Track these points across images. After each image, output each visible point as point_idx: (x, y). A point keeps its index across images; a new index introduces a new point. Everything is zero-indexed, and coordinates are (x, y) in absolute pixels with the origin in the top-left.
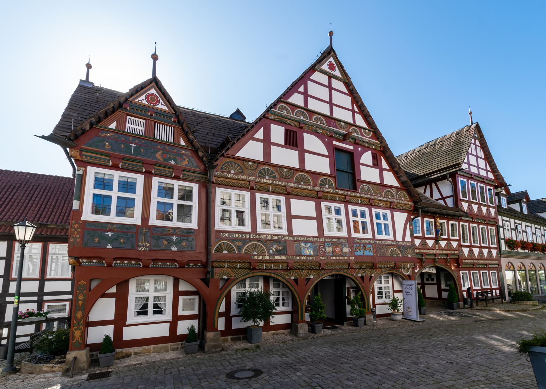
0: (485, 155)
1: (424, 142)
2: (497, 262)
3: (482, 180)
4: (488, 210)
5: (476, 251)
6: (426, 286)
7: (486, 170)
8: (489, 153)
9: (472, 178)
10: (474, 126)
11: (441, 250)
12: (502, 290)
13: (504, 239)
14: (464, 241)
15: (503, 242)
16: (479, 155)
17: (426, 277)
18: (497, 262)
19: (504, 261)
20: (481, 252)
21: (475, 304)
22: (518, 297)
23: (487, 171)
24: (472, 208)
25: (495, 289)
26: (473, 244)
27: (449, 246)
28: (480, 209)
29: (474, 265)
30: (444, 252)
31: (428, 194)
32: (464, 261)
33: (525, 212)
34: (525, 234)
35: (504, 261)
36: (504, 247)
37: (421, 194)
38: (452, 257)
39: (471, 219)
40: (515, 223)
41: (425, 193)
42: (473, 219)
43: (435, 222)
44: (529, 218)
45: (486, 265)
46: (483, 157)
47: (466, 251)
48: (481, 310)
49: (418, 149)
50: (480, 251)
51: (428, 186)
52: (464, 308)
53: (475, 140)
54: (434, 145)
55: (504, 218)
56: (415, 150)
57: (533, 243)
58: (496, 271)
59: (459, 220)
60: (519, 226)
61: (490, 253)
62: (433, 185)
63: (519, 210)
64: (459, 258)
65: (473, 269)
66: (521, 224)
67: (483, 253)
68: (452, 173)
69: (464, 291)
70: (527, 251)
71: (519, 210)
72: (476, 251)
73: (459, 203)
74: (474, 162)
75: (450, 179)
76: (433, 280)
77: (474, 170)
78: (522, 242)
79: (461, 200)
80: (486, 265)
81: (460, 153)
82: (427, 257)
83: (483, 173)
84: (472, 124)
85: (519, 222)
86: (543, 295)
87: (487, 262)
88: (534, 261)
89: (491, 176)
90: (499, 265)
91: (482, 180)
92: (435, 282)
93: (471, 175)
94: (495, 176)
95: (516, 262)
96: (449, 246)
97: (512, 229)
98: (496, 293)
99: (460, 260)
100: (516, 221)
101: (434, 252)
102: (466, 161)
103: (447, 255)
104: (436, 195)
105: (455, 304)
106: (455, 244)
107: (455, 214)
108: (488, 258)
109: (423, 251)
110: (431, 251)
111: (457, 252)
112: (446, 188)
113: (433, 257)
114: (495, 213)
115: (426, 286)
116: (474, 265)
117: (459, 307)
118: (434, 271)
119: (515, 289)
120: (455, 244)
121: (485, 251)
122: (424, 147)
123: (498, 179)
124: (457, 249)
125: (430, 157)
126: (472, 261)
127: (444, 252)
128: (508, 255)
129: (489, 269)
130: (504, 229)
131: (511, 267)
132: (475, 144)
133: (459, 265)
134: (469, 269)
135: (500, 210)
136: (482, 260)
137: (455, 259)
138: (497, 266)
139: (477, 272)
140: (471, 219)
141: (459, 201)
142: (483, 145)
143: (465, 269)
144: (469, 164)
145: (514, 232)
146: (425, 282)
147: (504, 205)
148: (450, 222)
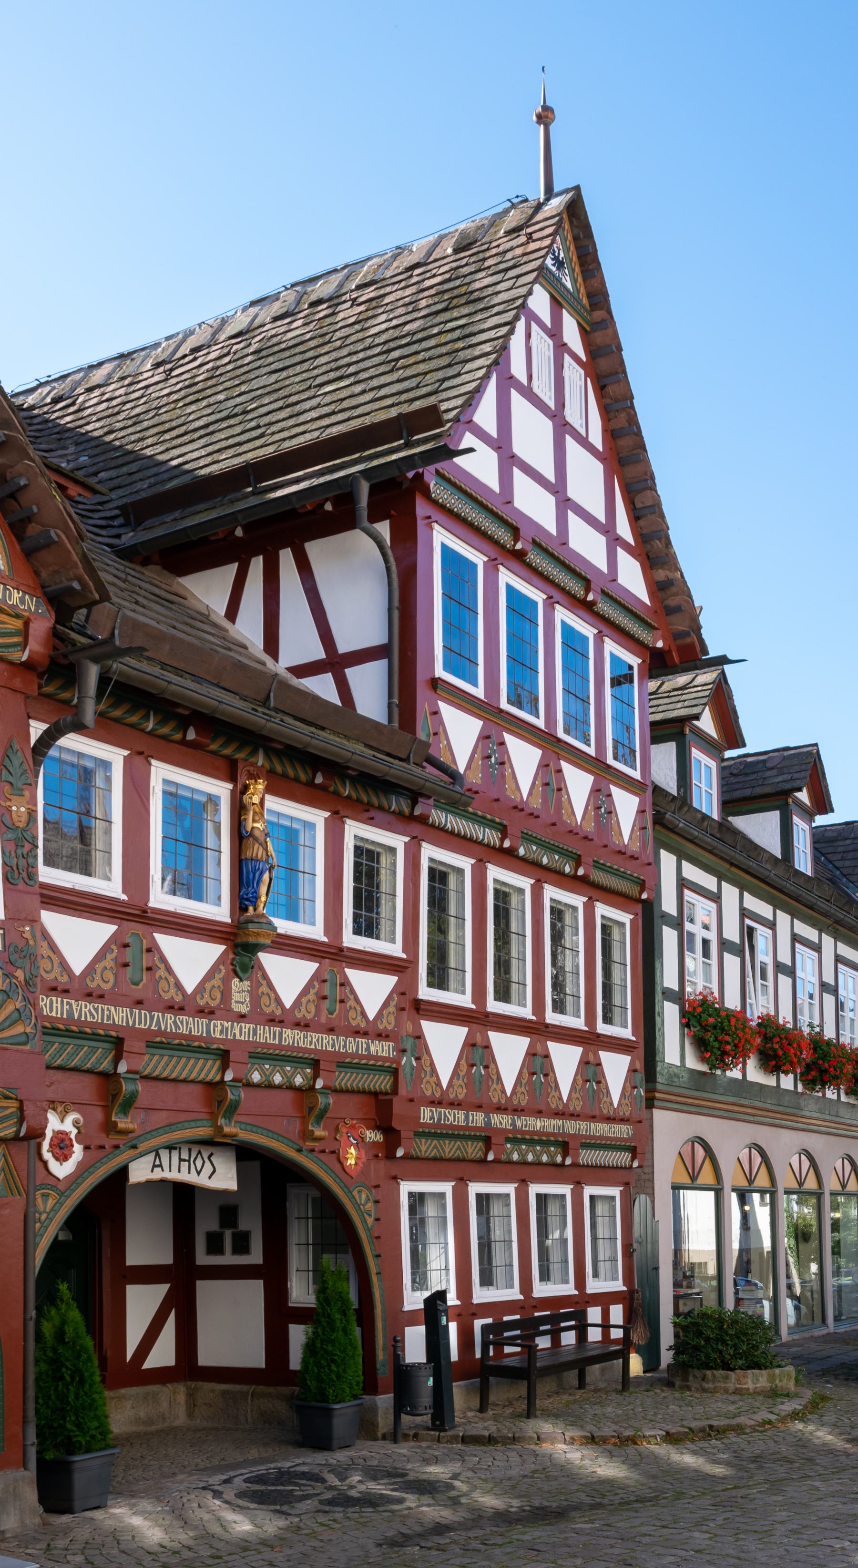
0: (610, 433)
1: (276, 275)
2: (623, 1131)
3: (576, 588)
4: (599, 797)
5: (509, 1052)
6: (205, 1289)
7: (607, 529)
8: (633, 420)
9: (519, 556)
10: (556, 204)
11: (272, 1021)
12: (639, 1303)
13: (678, 997)
14: (438, 979)
15: (670, 1015)
16: (573, 415)
17: (205, 1223)
18: (623, 1131)
19: (670, 1129)
20: (537, 1065)
21: (460, 1395)
22: (715, 1341)
23: (614, 541)
24: (504, 762)
25: (605, 1300)
26: (493, 1006)
27: (329, 1000)
28: (550, 780)
29: (490, 1145)
30: (291, 1037)
31: (249, 628)
32: (427, 1115)
33: (804, 862)
34: (785, 981)
35: (670, 1129)
36: (675, 1048)
37: (205, 617)
38: (346, 1079)
39: (490, 836)
40: (744, 913)
41: (232, 613)
42: (504, 832)
43: (239, 809)
44: (811, 898)
45: (565, 1147)
46: (596, 438)
47: (445, 1043)
48: (490, 1440)
49: (241, 322)
50: (531, 1054)
51: (257, 565)
52: (394, 1436)
53: (556, 304)
54: (334, 300)
55: (691, 872)
56: (224, 322)
57: (818, 1043)
58: (615, 1191)
59: (418, 827)
60: (762, 934)
61: (591, 1071)
62: (286, 558)
63: (774, 847)
64: (395, 1090)
65: (484, 1169)
66: (772, 925)
67: (548, 1071)
68: (388, 479)
69: (412, 1318)
70: (787, 1082)
71: (774, 847)
72: (509, 1052)
73: (423, 707)
74: (522, 444)
75: (384, 528)
76: (242, 1245)
77: (534, 504)
78: (768, 1024)
79: (435, 683)
80: (565, 1147)
81: (455, 361)
82: (158, 1064)
83: (587, 544)
84: (550, 192)
85: (764, 909)
86: (842, 1329)
87: (571, 1127)
88: (816, 1143)
89: (632, 578)
90: (634, 1152)
91: (576, 588)
92: (256, 1256)
93: (516, 532)
94: (657, 588)
95: (731, 1140)
96: (329, 1000)
97: (725, 945)
98: (606, 1326)
99: (398, 1107)
100: (753, 903)
101: (218, 1029)
102: (485, 414)
103: (315, 1063)
104: (300, 643)
105: (343, 1413)
106: (372, 990)
107: (374, 774)
108: (577, 1106)
109: (120, 1016)
110: (192, 1026)
111: (382, 1049)
112: (351, 584)
113: (209, 1070)
114: (639, 826)
115: (205, 1289)
116: (490, 1145)
117: (366, 1428)
118: (221, 1176)
119: (714, 1296)
120: (372, 990)
121: (565, 1059)
122: (276, 308)
123: (671, 611)
124: (388, 1024)
125: (295, 379)
126: (478, 1119)
127: (291, 1037)
128: (698, 1094)
129: (579, 1176)
130: (685, 943)
131: (700, 1167)
132: (555, 332)
133: (392, 1137)
134: (462, 1170)
135: (668, 816)
136: (539, 1113)
137: (375, 1094)
138: (622, 1158)
139: (509, 1189)
140: (490, 836)
141: (422, 692)
142: (604, 364)
143: (434, 1167)
144: (509, 461)
145: (732, 962)
146: (203, 1259)
147: (707, 797)
148: (354, 830)
